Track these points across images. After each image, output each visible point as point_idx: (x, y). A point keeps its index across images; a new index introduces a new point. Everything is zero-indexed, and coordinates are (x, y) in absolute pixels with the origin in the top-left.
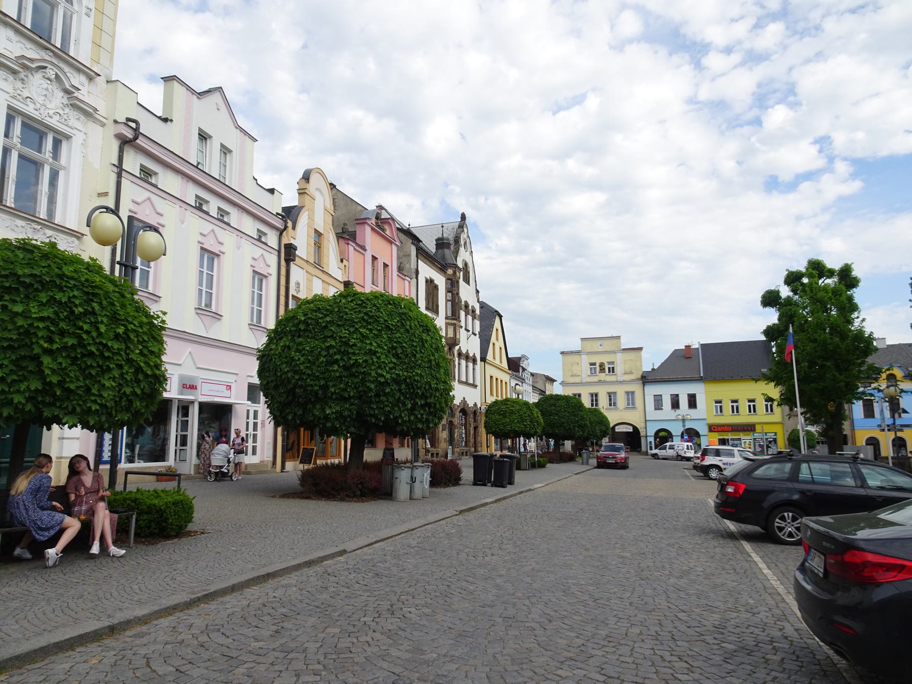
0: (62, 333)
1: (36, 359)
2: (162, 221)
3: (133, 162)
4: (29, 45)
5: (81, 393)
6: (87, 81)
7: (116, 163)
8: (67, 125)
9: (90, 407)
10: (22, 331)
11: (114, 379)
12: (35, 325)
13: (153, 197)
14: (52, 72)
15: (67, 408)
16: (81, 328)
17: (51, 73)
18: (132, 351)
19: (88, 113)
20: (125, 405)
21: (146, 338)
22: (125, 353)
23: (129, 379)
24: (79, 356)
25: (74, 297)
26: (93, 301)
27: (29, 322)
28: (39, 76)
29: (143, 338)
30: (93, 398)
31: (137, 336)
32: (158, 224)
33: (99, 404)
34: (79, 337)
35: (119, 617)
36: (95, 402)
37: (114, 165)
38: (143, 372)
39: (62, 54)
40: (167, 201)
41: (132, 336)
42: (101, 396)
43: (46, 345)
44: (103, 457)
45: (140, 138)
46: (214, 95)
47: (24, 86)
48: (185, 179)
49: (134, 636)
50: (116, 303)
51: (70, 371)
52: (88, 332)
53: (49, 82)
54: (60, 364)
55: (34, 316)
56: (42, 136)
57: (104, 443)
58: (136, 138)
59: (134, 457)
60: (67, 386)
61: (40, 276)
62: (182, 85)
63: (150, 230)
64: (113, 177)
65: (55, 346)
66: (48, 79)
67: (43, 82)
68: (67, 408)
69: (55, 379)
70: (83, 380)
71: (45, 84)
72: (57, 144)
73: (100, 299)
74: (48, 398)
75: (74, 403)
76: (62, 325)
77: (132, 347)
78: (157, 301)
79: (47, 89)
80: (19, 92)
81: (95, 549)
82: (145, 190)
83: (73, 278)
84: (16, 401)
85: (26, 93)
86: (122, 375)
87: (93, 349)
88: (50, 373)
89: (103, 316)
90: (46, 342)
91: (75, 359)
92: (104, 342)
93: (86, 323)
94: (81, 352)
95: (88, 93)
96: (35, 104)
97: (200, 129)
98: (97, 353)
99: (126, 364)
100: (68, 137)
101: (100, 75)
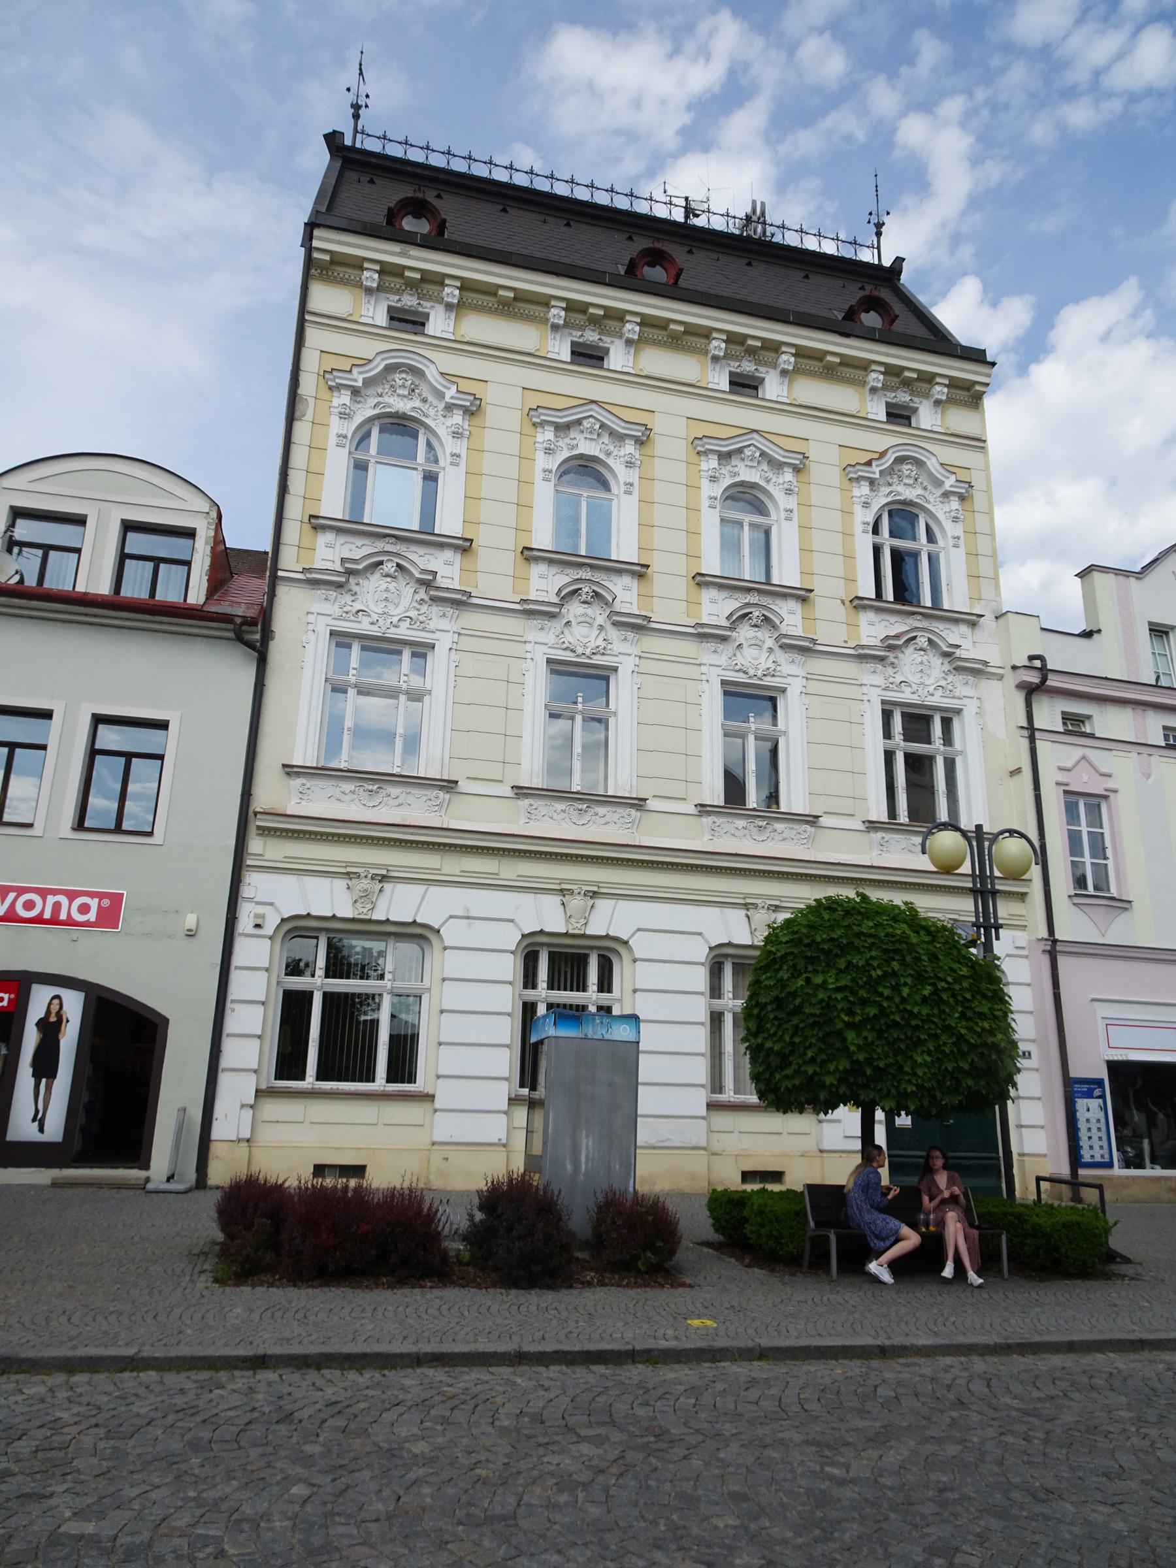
0: (863, 1002)
1: (839, 1034)
2: (1111, 784)
3: (1048, 715)
4: (893, 619)
5: (892, 1071)
6: (970, 629)
7: (1025, 724)
8: (954, 697)
9: (905, 1089)
10: (824, 1004)
11: (929, 1053)
12: (833, 996)
13: (1093, 755)
14: (923, 640)
15: (881, 1090)
16: (881, 995)
17: (922, 641)
18: (949, 1015)
19: (977, 671)
20: (951, 1085)
21: (968, 996)
22: (940, 1018)
23: (948, 1051)
24: (884, 1028)
25: (872, 958)
26: (893, 959)
27: (828, 994)
28: (910, 650)
29: (964, 997)
30: (907, 1078)
31: (953, 996)
32: (1106, 790)
33: (916, 1085)
34: (880, 1006)
35: (899, 1340)
36: (909, 1081)
37: (1022, 727)
38: (967, 1042)
39: (937, 612)
40: (1114, 753)
41: (945, 996)
42: (915, 1074)
43: (846, 1019)
44: (1082, 1156)
45: (1050, 676)
46: (1166, 561)
47: (895, 670)
48: (1139, 710)
49: (904, 1365)
50: (923, 957)
51: (877, 1046)
52: (888, 998)
53: (922, 653)
54: (866, 1038)
55: (831, 986)
56: (927, 719)
57: (1080, 1134)
58: (1044, 679)
59: (1143, 1159)
60: (875, 1064)
61: (838, 939)
62: (1107, 573)
63: (1011, 836)
64: (1025, 744)
65: (857, 1019)
66: (921, 649)
67: (915, 656)
68: (881, 1090)
69: (861, 1057)
70: (894, 1055)
71: (918, 657)
72: (947, 723)
73: (903, 955)
74: (860, 1079)
75: (888, 1084)
76: (862, 993)
77: (947, 1010)
78: (1126, 909)
79: (922, 663)
80: (891, 680)
81: (948, 1272)
82: (1072, 747)
83: (871, 936)
84: (828, 1083)
85: (899, 678)
86: (938, 1048)
87: (897, 1018)
88: (855, 1049)
89: (907, 977)
90: (846, 1015)
91: (880, 1032)
92: (909, 1008)
93: (886, 987)
94: (886, 1023)
95: (970, 645)
96: (910, 686)
97: (1150, 623)
98: (903, 1023)
99: (943, 1032)
100: (958, 712)
101: (983, 616)
